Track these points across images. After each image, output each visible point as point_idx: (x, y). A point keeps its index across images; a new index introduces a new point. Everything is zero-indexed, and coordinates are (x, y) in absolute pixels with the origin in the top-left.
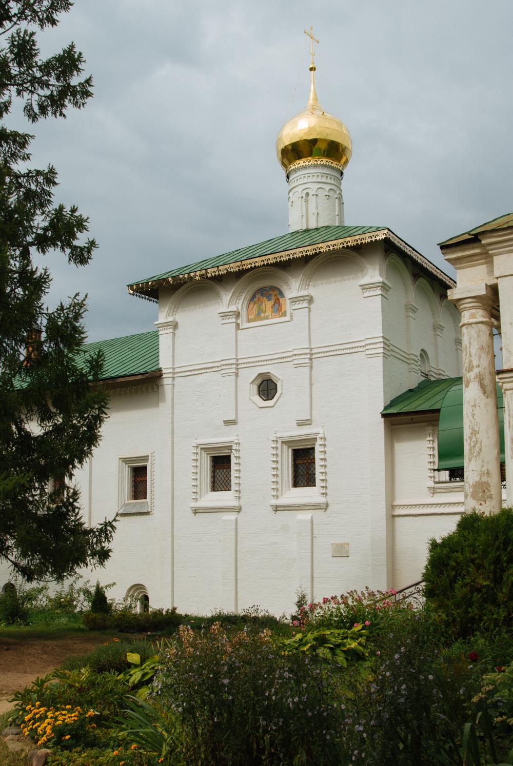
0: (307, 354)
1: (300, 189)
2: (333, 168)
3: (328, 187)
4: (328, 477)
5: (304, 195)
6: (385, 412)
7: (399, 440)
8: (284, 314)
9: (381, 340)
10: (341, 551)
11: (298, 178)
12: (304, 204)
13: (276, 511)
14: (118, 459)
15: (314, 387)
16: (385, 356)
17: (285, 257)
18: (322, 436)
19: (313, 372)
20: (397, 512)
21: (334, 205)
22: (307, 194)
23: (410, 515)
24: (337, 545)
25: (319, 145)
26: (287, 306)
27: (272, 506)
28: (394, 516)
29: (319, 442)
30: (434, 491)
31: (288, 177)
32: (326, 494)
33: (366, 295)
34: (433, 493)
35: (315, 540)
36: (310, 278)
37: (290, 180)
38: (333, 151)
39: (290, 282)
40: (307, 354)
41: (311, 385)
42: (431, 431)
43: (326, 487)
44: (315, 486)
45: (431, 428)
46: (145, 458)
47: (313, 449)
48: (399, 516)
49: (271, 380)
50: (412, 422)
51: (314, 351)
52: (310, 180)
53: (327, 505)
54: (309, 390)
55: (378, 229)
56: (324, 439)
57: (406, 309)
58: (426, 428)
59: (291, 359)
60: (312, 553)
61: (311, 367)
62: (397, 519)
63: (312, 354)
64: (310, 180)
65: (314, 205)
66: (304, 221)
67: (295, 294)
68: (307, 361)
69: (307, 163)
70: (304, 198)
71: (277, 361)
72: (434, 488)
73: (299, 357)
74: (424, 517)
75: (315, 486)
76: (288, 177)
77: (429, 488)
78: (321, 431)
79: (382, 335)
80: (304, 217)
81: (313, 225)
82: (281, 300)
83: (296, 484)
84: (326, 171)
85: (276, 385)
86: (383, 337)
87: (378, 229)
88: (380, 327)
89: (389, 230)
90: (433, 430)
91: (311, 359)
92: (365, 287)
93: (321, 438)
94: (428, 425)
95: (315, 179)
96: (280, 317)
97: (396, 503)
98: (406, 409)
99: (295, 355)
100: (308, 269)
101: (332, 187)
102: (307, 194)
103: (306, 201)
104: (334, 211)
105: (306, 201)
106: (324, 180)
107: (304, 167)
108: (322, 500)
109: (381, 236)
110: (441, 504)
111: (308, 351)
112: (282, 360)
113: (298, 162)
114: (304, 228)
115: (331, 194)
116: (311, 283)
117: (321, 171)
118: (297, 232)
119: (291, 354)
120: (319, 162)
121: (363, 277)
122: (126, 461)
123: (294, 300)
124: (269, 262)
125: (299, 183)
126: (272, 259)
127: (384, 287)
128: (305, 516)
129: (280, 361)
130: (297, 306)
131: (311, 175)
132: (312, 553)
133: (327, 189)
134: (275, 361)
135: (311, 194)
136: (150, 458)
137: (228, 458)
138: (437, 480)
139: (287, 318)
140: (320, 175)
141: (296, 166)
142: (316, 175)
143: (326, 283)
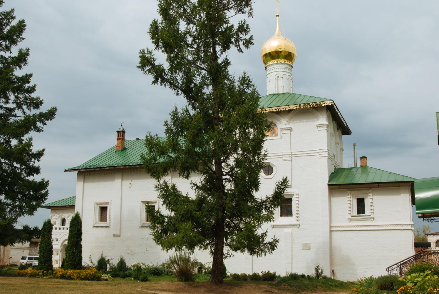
0: (289, 155)
1: (274, 74)
2: (286, 64)
3: (288, 74)
4: (300, 212)
5: (276, 77)
6: (329, 184)
7: (333, 197)
8: (277, 135)
9: (327, 150)
10: (306, 247)
11: (273, 68)
12: (277, 81)
13: (273, 227)
14: (94, 203)
15: (293, 170)
16: (328, 158)
17: (281, 109)
18: (297, 193)
19: (292, 163)
20: (333, 229)
21: (290, 83)
22: (278, 77)
23: (339, 231)
24: (304, 244)
25: (282, 53)
26: (279, 132)
27: (271, 225)
28: (331, 231)
29: (295, 196)
30: (350, 220)
31: (266, 68)
32: (299, 220)
33: (319, 129)
34: (350, 221)
35: (293, 242)
36: (291, 119)
37: (267, 69)
38: (289, 56)
39: (281, 121)
40: (289, 155)
41: (291, 169)
42: (349, 193)
43: (299, 217)
44: (292, 216)
45: (350, 191)
46: (107, 203)
47: (291, 199)
48: (334, 231)
49: (270, 166)
50: (340, 188)
51: (293, 154)
52: (279, 70)
53: (300, 225)
54: (290, 171)
55: (327, 100)
56: (298, 194)
57: (331, 135)
58: (347, 191)
59: (282, 156)
60: (292, 247)
61: (291, 161)
62: (332, 232)
63: (292, 155)
64: (279, 70)
65: (282, 82)
66: (277, 90)
67: (283, 126)
68: (290, 158)
69: (278, 62)
70: (277, 78)
71: (274, 157)
72: (351, 219)
73: (285, 156)
74: (340, 232)
75: (292, 216)
76: (266, 68)
77: (349, 219)
78: (297, 191)
79: (327, 148)
80: (277, 87)
81: (281, 92)
82: (275, 128)
83: (281, 216)
84: (286, 66)
85: (273, 168)
86: (328, 150)
87: (327, 100)
88: (326, 145)
89: (333, 101)
90: (350, 192)
91: (291, 157)
92: (318, 126)
93: (297, 194)
94: (348, 190)
95: (282, 70)
96: (275, 136)
97: (332, 225)
98: (338, 183)
99: (284, 155)
100: (290, 115)
101: (290, 74)
102: (278, 77)
103: (277, 80)
104: (290, 86)
105: (277, 80)
106: (286, 70)
107: (276, 64)
108: (297, 223)
109: (330, 103)
110: (354, 226)
111: (290, 153)
112: (276, 157)
113: (273, 61)
114: (277, 93)
115: (289, 77)
116: (291, 122)
117: (285, 66)
118: (273, 95)
119: (282, 154)
120: (284, 62)
121: (317, 121)
122: (98, 204)
123: (283, 129)
124: (273, 111)
125: (273, 71)
126: (274, 109)
127: (328, 127)
128: (289, 230)
129: (275, 157)
130: (284, 132)
131: (280, 68)
132: (292, 247)
133: (287, 75)
134: (273, 157)
135: (280, 77)
136: (157, 202)
137: (106, 208)
138: (352, 215)
139: (279, 137)
140: (284, 68)
141: (273, 63)
142: (282, 68)
143: (298, 122)
